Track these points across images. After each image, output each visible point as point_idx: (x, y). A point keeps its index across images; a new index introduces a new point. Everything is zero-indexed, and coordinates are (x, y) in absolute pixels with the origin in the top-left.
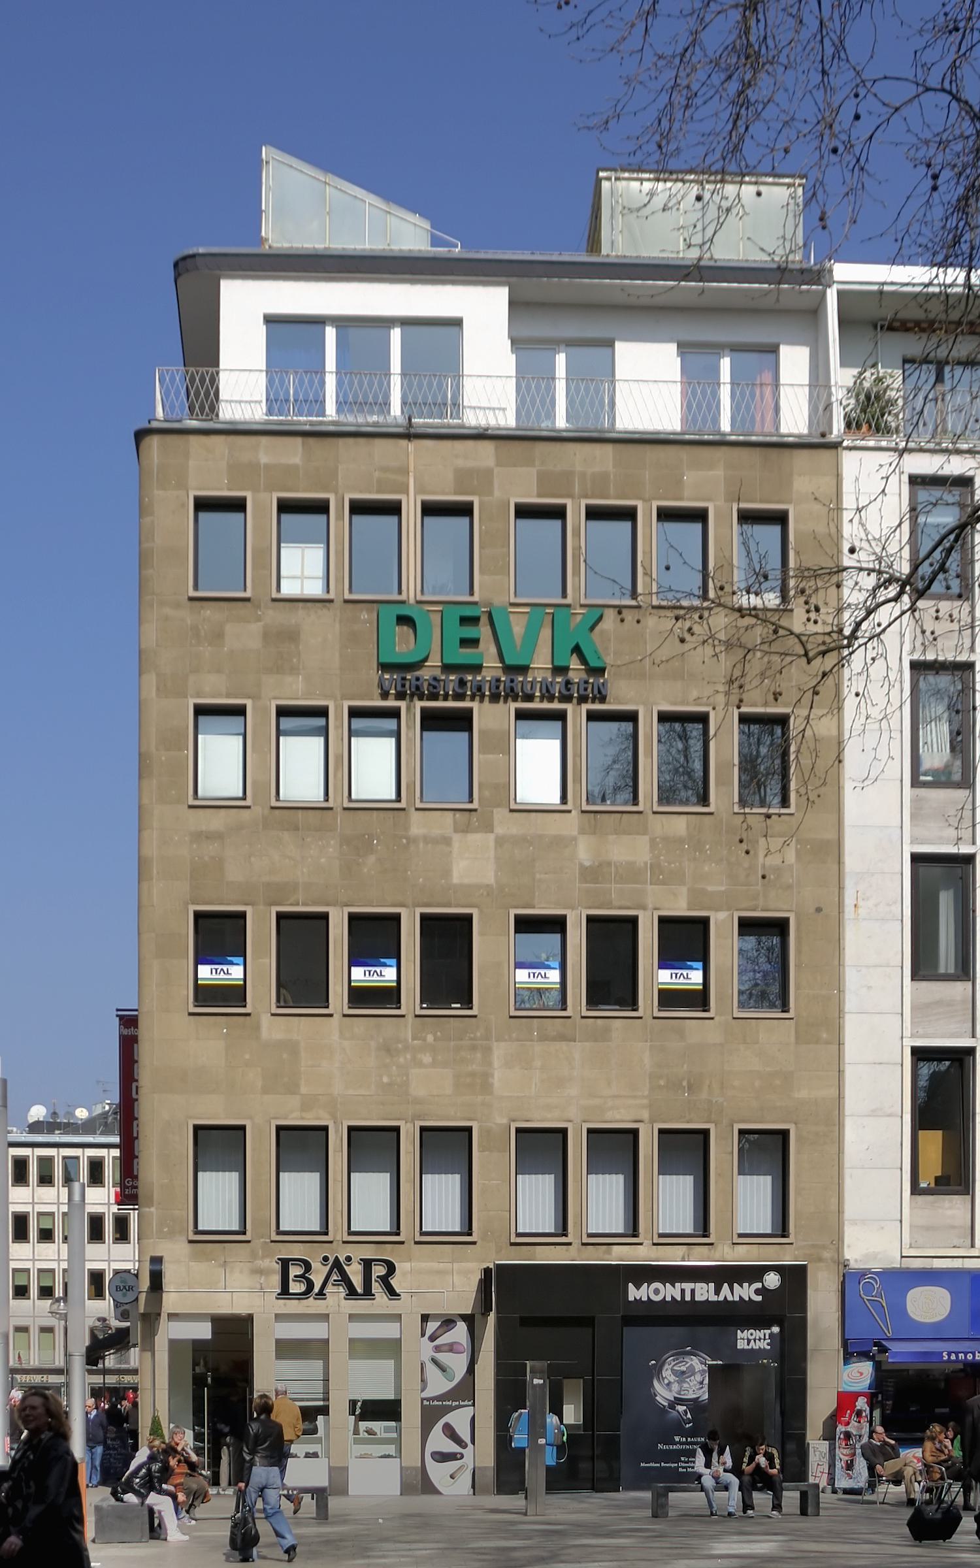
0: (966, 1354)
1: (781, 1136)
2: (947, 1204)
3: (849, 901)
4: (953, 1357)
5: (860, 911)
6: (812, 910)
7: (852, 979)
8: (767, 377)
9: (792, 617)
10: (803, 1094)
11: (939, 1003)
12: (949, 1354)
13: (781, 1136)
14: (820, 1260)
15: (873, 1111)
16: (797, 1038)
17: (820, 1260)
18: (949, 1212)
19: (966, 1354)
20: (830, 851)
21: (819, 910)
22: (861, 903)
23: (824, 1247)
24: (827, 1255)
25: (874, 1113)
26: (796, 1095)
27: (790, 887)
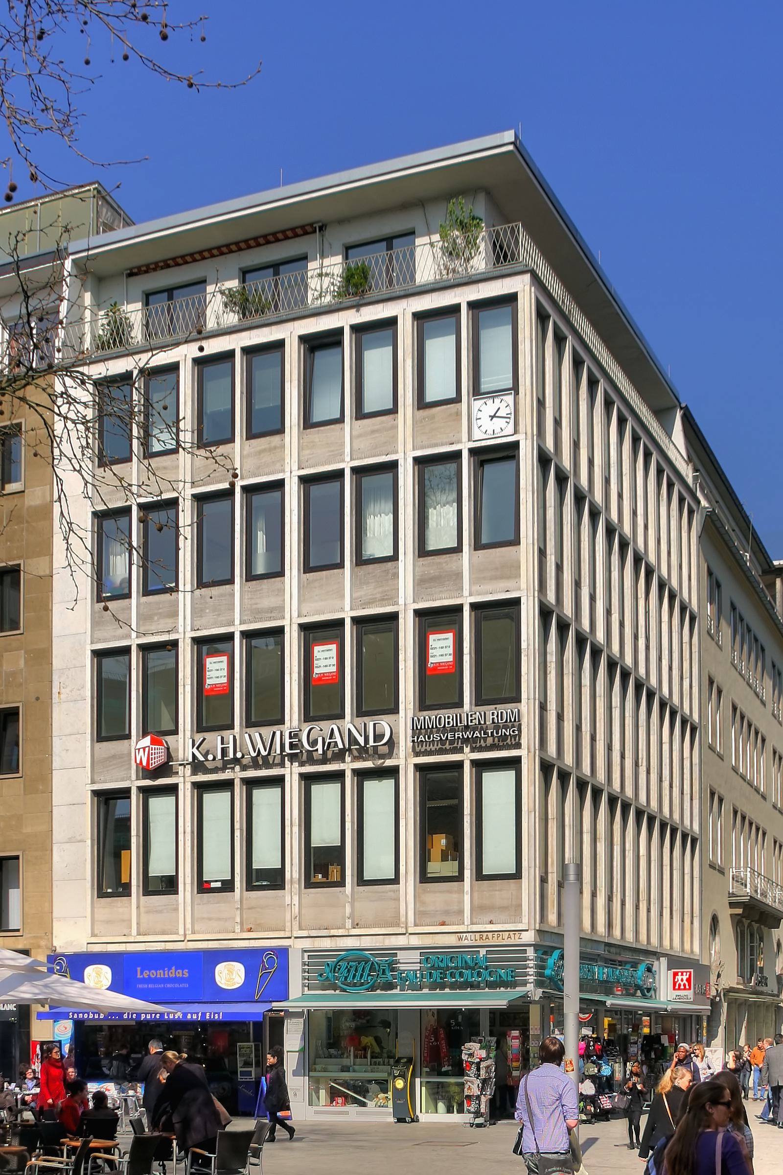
0: (192, 1014)
1: (513, 871)
2: (119, 904)
3: (55, 690)
4: (96, 1017)
5: (62, 696)
6: (34, 700)
7: (57, 745)
8: (181, 336)
9: (24, 496)
10: (28, 830)
11: (114, 757)
12: (168, 1015)
13: (513, 871)
14: (39, 947)
15: (70, 839)
16: (25, 791)
17: (39, 947)
18: (121, 910)
19: (192, 1014)
20: (42, 657)
21: (37, 699)
22: (63, 691)
23: (41, 938)
24: (43, 943)
25: (71, 841)
26: (24, 831)
27: (21, 684)
